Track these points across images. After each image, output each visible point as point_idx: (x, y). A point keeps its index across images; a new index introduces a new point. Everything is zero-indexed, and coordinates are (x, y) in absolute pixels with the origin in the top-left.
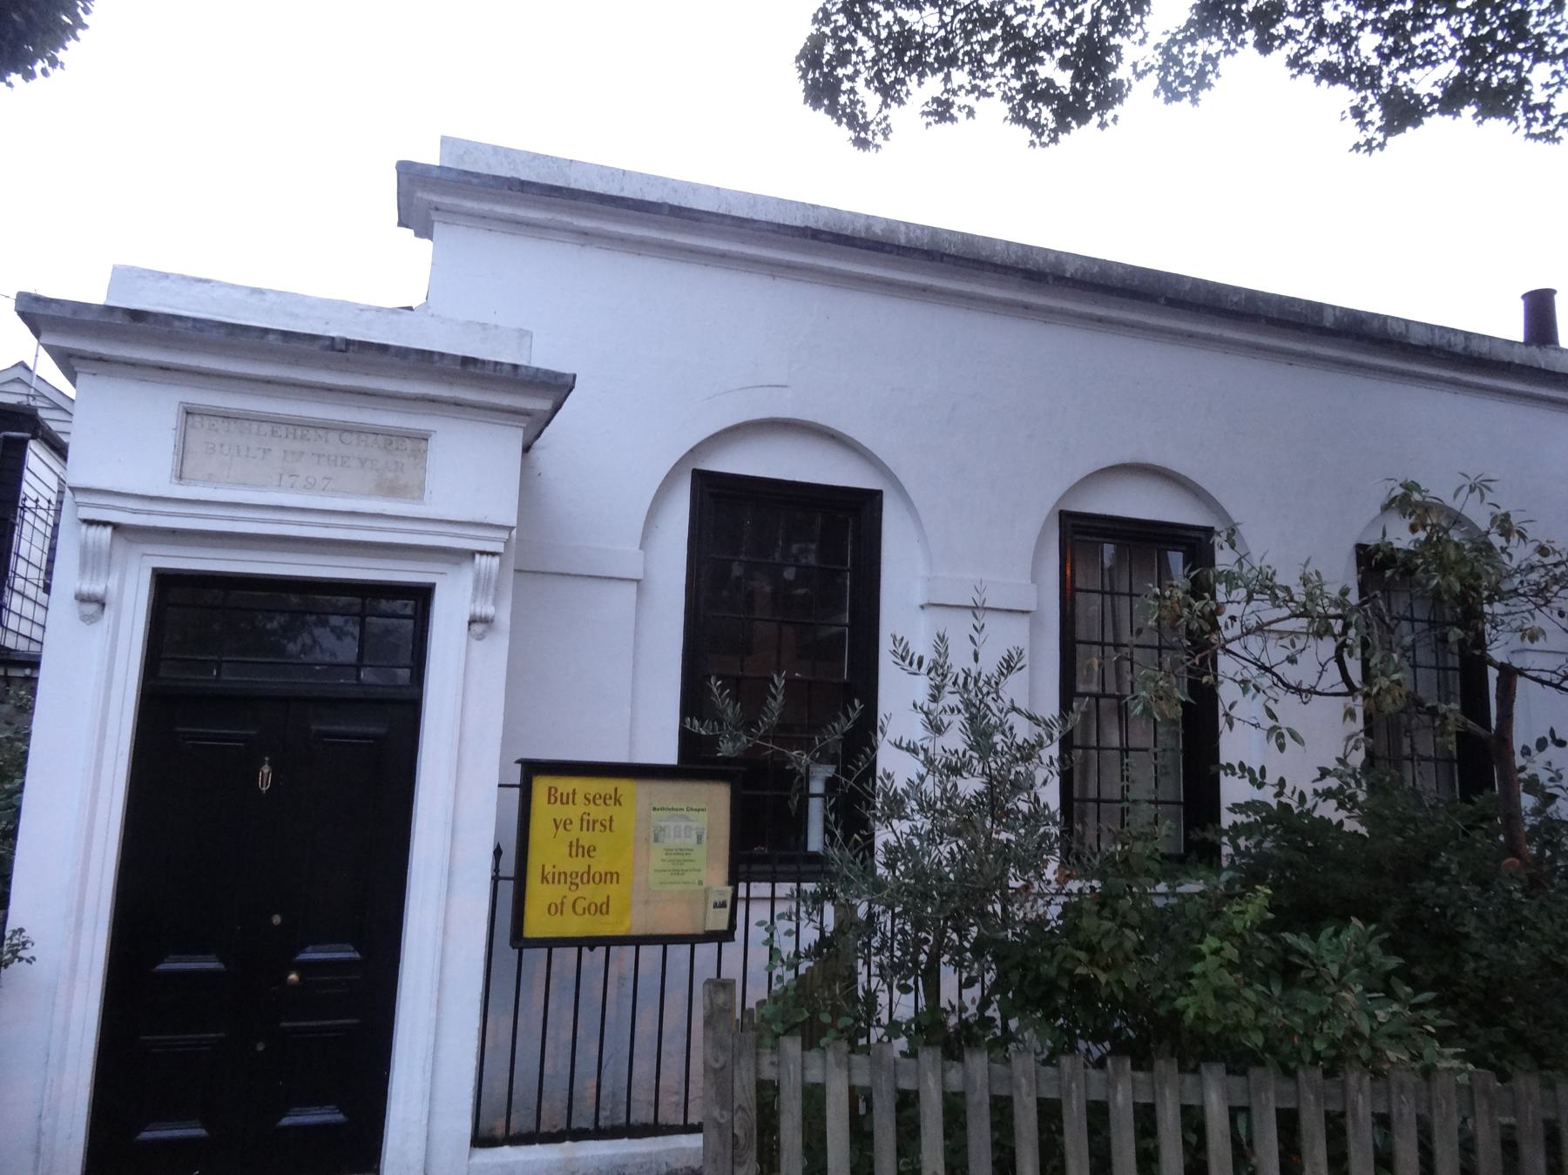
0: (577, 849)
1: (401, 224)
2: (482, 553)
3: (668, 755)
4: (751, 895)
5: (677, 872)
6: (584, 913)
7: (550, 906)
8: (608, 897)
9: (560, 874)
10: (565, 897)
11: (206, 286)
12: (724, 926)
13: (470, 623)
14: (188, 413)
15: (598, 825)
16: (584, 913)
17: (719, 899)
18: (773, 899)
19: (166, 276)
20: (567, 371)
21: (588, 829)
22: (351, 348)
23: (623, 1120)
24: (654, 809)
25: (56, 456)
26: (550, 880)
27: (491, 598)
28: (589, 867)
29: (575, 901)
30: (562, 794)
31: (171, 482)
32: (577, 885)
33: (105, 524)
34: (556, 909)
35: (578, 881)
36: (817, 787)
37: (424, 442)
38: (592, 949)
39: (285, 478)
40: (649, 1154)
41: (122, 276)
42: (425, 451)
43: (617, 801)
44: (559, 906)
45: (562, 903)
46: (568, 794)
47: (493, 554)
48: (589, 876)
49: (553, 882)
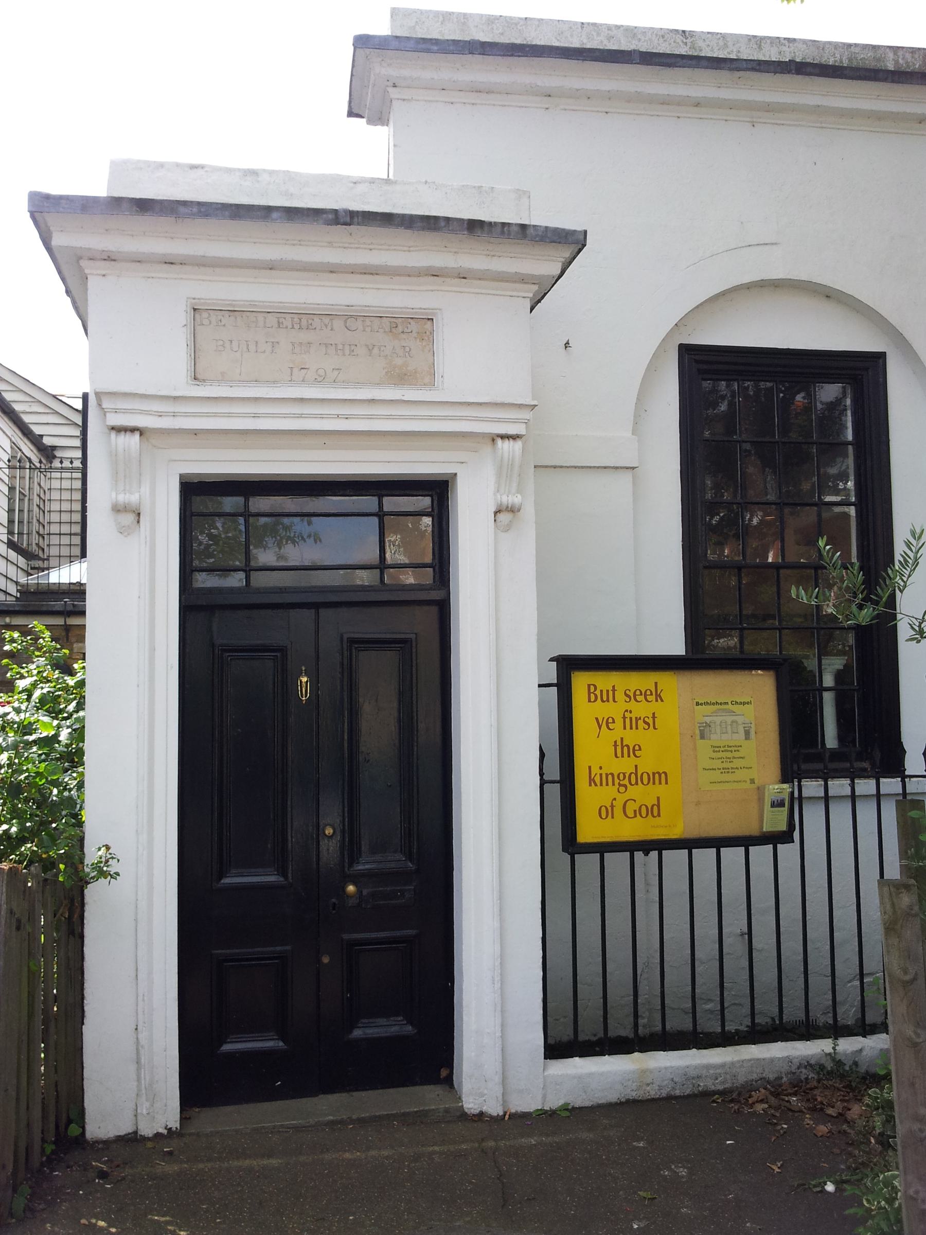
0: (622, 749)
1: (351, 114)
2: (503, 437)
3: (676, 646)
4: (831, 793)
5: (726, 771)
6: (635, 816)
7: (601, 807)
8: (658, 798)
9: (607, 775)
10: (615, 799)
11: (200, 172)
12: (783, 827)
13: (496, 513)
14: (195, 310)
15: (641, 722)
16: (635, 816)
17: (780, 797)
18: (827, 799)
19: (161, 165)
20: (579, 229)
21: (631, 728)
22: (356, 220)
23: (659, 1028)
24: (698, 704)
25: (6, 419)
26: (598, 783)
27: (514, 485)
28: (636, 766)
29: (629, 800)
30: (601, 691)
31: (187, 383)
32: (625, 786)
33: (133, 430)
34: (606, 812)
35: (626, 782)
36: (828, 680)
37: (429, 322)
38: (646, 853)
39: (295, 371)
40: (723, 1066)
41: (118, 168)
42: (432, 333)
43: (659, 697)
44: (610, 809)
45: (612, 806)
46: (608, 691)
47: (515, 437)
48: (636, 777)
49: (601, 784)
